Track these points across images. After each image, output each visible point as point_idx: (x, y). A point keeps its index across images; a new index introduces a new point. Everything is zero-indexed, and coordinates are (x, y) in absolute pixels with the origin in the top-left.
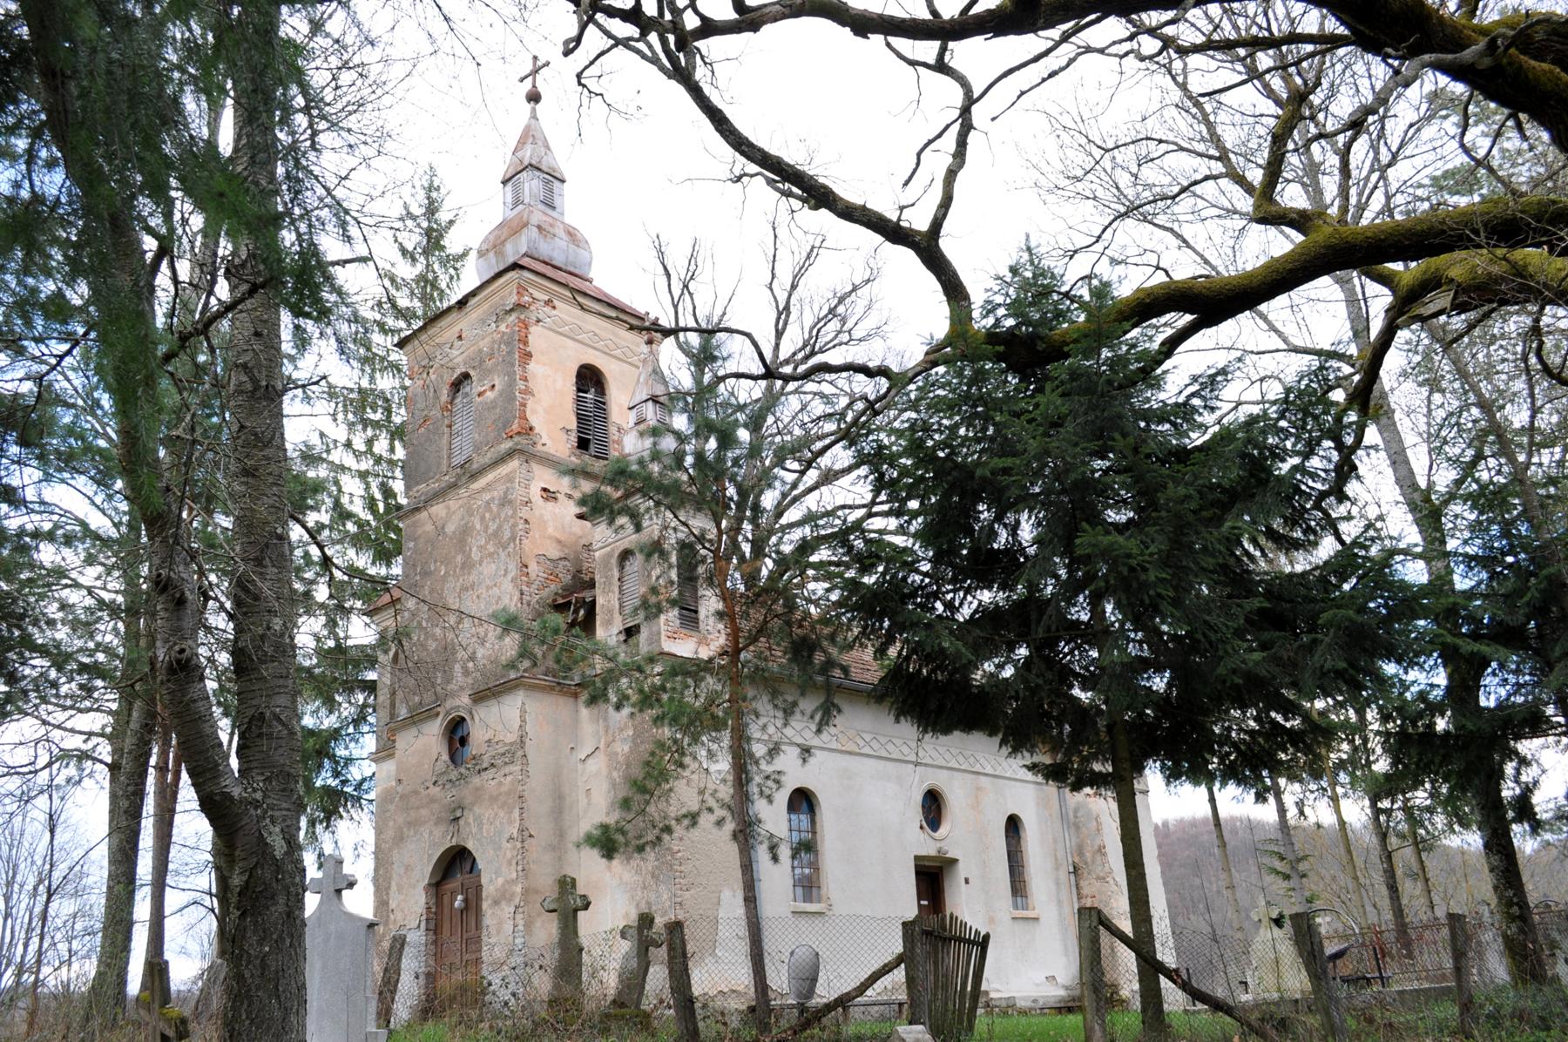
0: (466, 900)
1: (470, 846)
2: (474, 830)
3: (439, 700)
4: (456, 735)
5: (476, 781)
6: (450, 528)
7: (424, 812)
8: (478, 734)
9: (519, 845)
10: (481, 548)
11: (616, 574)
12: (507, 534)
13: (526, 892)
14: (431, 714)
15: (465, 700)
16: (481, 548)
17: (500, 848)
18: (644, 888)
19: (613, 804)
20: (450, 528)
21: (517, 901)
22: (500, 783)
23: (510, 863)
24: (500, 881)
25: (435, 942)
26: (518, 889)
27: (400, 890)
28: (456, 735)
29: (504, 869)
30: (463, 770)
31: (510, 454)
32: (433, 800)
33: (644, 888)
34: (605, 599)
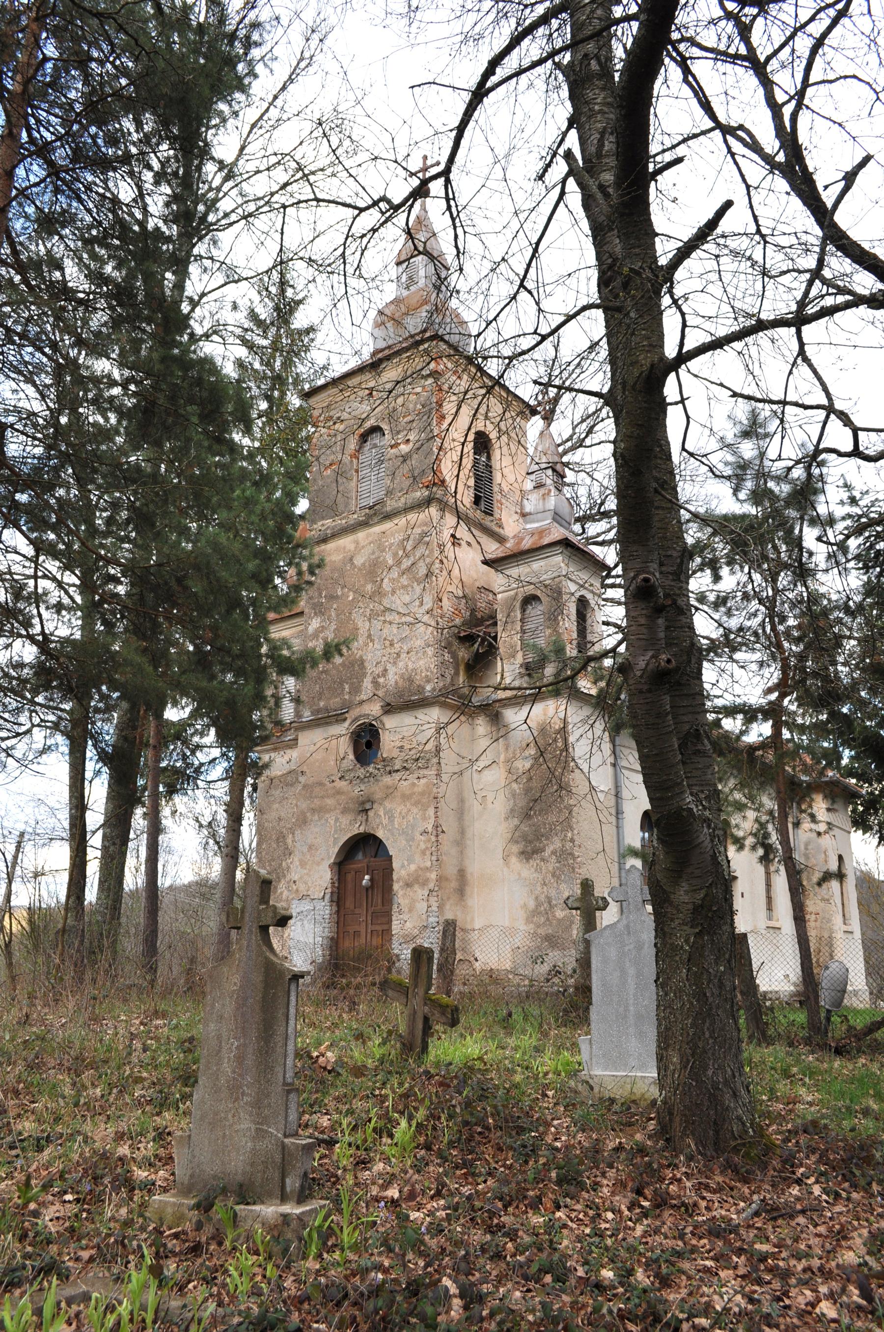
0: (371, 880)
1: (380, 834)
2: (385, 821)
3: (348, 706)
4: (366, 742)
5: (387, 780)
6: (359, 561)
7: (330, 802)
8: (388, 743)
9: (433, 839)
10: (392, 580)
11: (519, 616)
12: (423, 571)
13: (440, 879)
14: (339, 718)
15: (375, 709)
16: (392, 580)
17: (413, 839)
18: (545, 884)
19: (512, 811)
20: (359, 561)
21: (431, 886)
22: (414, 784)
23: (423, 853)
24: (413, 867)
25: (338, 912)
26: (433, 876)
27: (303, 864)
28: (366, 742)
29: (417, 858)
30: (371, 769)
31: (428, 502)
32: (339, 792)
33: (545, 884)
34: (508, 638)
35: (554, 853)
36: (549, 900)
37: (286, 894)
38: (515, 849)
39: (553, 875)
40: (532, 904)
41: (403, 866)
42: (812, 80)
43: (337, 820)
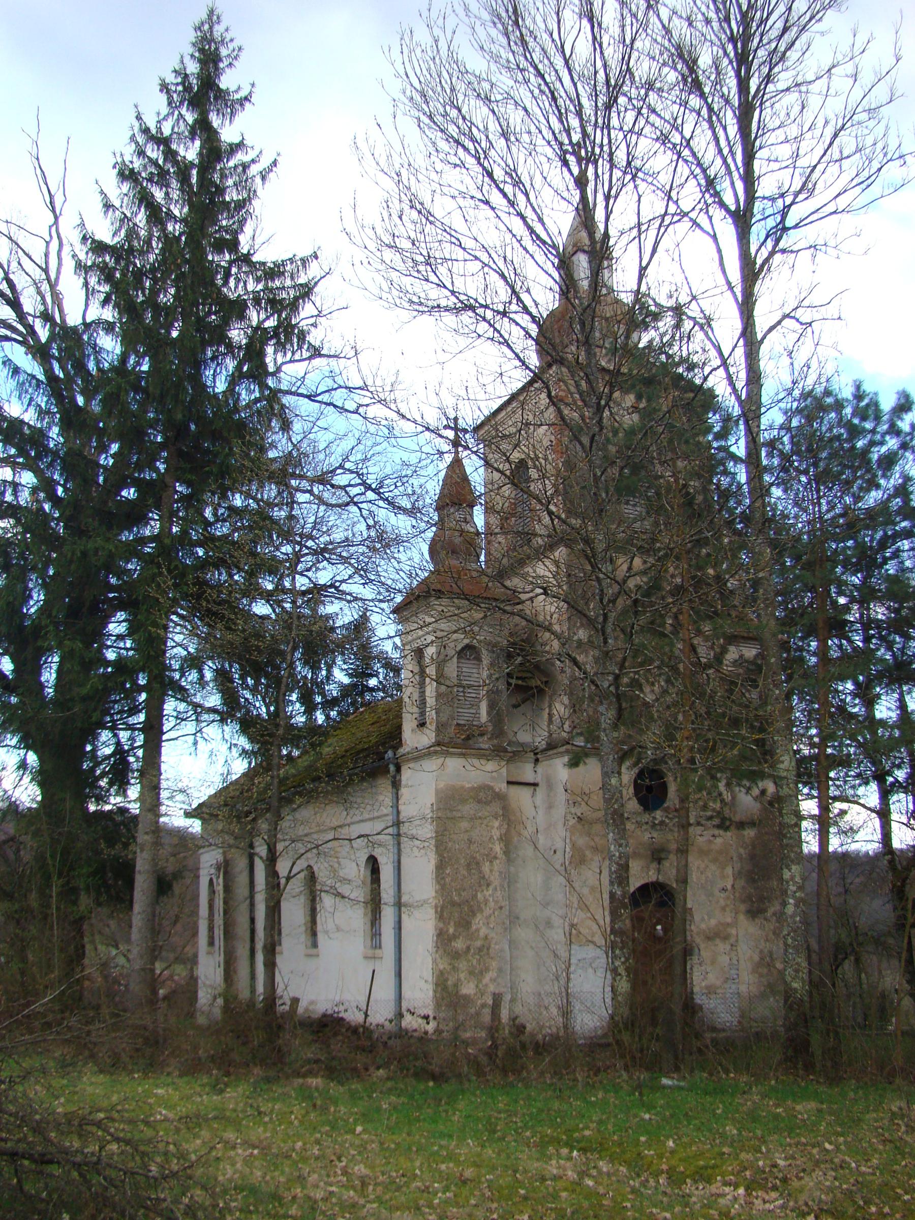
19: (740, 873)
24: (713, 922)
30: (658, 814)
35: (774, 914)
36: (771, 953)
37: (483, 931)
38: (743, 907)
39: (774, 933)
40: (756, 958)
41: (703, 919)
42: (637, 240)
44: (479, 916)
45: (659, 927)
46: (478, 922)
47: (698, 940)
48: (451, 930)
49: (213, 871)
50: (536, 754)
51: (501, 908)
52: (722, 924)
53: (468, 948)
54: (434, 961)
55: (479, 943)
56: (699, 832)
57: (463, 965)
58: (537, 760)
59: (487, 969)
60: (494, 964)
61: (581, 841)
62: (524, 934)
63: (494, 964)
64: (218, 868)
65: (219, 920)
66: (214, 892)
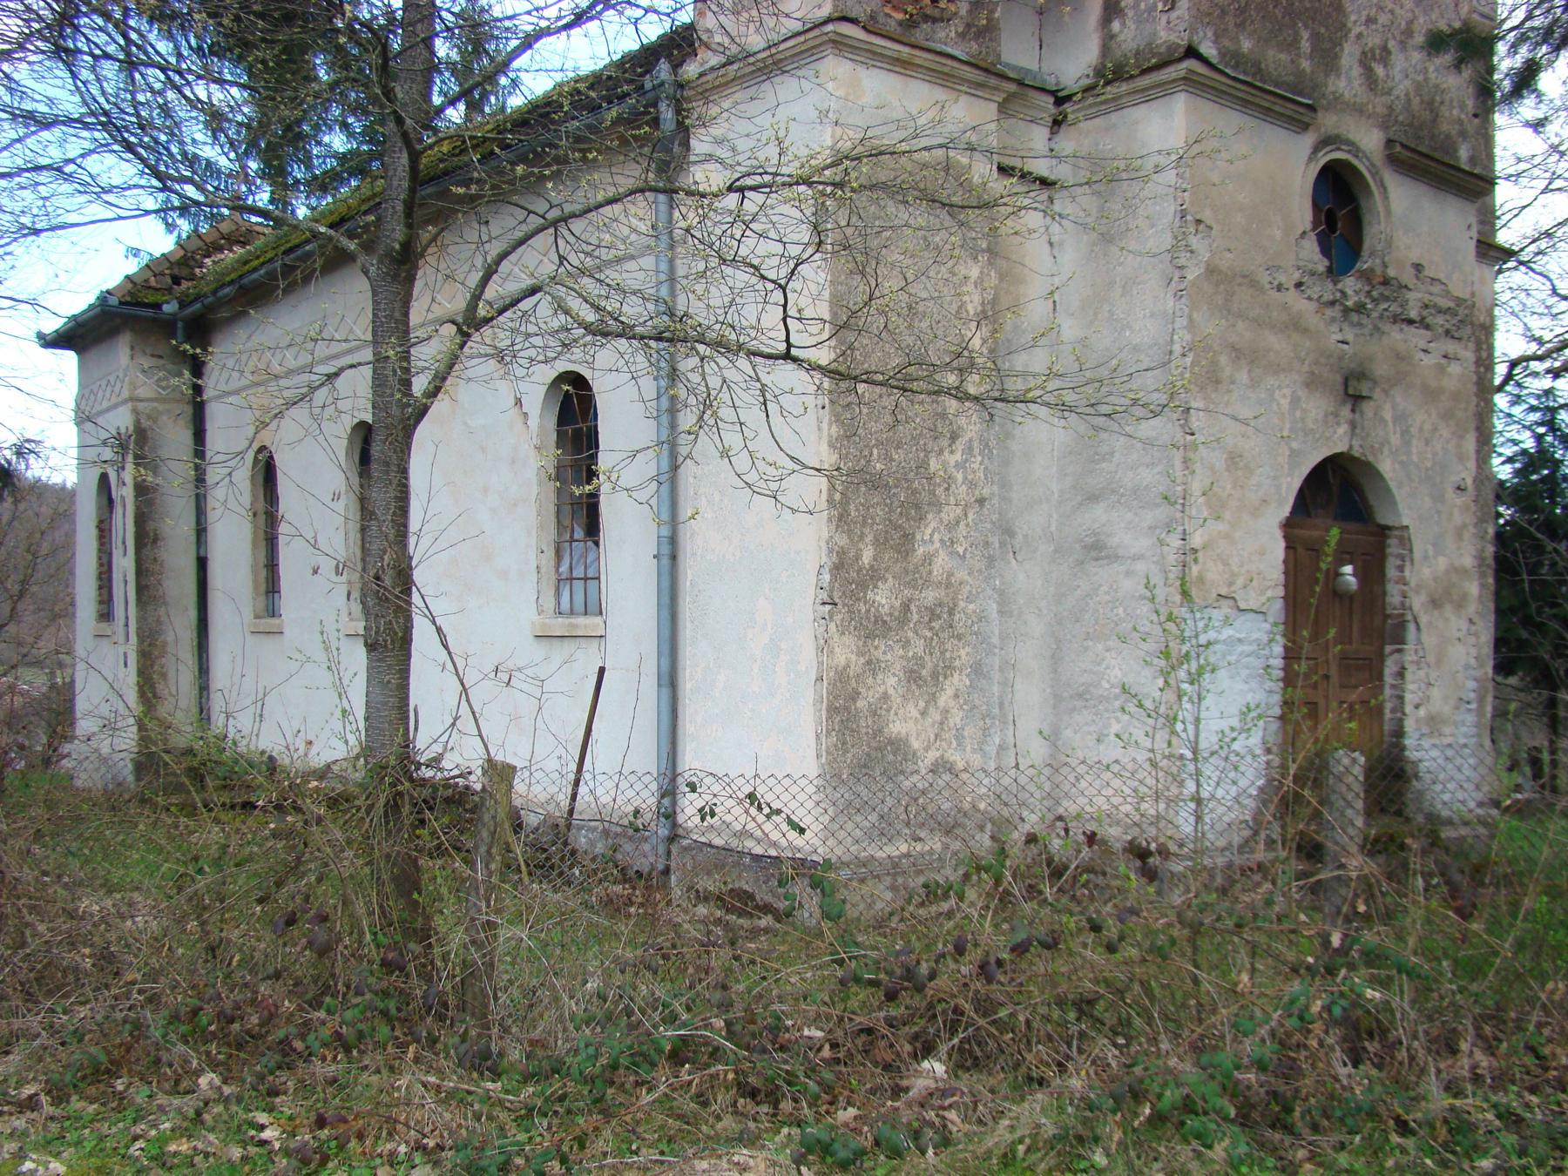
30: (1350, 284)
37: (942, 563)
43: (1295, 401)
44: (932, 522)
45: (1348, 569)
46: (929, 535)
47: (1417, 602)
48: (867, 556)
49: (108, 454)
50: (1060, 101)
51: (981, 501)
52: (1456, 570)
53: (906, 608)
54: (824, 647)
55: (930, 596)
56: (1422, 344)
57: (889, 653)
58: (1057, 124)
59: (950, 668)
60: (964, 654)
61: (1211, 326)
62: (1026, 576)
63: (964, 654)
64: (122, 444)
65: (124, 564)
66: (111, 501)
